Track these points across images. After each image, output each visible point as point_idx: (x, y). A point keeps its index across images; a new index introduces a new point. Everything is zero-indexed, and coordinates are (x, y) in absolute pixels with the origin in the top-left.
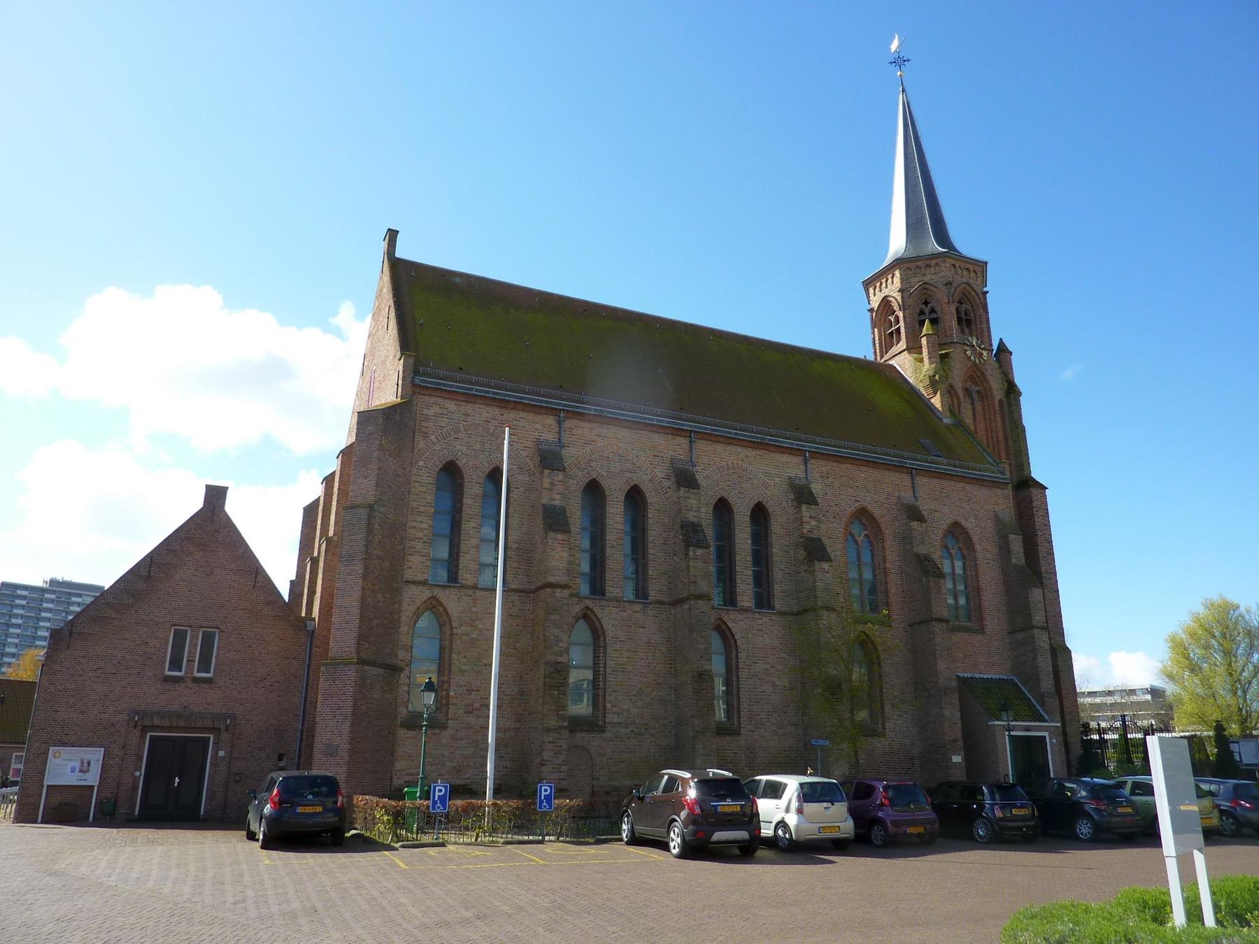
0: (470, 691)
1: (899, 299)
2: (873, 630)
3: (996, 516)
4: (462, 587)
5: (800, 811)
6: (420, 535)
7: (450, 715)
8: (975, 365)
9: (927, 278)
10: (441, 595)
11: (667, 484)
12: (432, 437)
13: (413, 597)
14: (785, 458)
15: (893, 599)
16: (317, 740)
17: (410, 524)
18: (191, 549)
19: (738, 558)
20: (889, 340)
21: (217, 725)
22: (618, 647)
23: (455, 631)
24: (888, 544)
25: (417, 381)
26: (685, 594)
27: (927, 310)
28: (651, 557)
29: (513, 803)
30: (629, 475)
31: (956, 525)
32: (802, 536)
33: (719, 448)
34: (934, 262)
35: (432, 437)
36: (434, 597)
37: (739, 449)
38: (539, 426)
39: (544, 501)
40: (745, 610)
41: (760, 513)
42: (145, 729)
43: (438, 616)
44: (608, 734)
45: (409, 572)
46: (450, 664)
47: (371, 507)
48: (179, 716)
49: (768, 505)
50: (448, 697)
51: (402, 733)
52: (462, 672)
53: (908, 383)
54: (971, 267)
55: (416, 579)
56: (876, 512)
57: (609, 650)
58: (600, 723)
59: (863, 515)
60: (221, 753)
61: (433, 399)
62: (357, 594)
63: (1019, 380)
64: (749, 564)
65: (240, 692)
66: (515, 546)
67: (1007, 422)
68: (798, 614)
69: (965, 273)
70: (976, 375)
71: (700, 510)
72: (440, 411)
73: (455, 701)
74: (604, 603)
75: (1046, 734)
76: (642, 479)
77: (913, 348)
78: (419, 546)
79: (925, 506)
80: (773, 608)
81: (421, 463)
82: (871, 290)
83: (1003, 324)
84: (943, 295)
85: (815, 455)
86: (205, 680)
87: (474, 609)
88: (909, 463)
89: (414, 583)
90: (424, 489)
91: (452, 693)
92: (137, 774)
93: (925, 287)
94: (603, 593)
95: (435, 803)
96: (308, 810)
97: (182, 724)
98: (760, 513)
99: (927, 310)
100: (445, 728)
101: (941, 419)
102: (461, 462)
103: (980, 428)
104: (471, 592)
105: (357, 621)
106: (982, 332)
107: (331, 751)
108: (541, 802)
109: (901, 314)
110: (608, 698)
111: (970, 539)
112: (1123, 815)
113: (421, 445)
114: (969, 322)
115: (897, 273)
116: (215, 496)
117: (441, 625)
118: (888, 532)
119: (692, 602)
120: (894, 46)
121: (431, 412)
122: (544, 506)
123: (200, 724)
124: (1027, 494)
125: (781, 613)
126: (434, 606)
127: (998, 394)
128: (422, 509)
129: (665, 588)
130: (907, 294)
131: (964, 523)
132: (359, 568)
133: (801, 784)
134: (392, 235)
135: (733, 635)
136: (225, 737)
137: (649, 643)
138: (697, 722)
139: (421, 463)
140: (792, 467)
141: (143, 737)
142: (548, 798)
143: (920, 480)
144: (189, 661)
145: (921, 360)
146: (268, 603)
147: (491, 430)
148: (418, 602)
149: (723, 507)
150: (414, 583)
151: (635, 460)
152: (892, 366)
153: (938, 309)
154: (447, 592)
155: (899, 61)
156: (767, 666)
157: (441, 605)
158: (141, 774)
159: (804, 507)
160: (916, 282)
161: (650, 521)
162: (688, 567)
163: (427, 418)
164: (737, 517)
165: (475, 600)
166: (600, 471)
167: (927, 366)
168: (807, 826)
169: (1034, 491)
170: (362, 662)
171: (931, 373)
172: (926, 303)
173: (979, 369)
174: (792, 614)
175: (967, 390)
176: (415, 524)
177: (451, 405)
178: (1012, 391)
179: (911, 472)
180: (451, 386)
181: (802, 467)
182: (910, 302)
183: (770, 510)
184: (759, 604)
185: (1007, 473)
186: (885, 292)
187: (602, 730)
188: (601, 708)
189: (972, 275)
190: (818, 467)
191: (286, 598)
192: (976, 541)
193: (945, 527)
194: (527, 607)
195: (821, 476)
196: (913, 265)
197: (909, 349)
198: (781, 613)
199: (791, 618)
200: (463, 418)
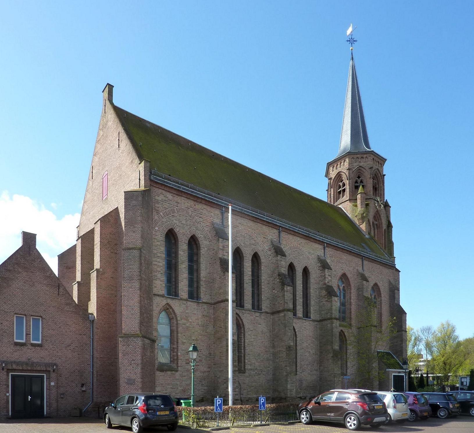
1: (347, 173)
2: (345, 330)
3: (390, 282)
4: (181, 299)
5: (395, 407)
6: (159, 269)
7: (179, 365)
9: (361, 164)
11: (269, 253)
12: (161, 214)
13: (159, 303)
14: (317, 246)
15: (353, 316)
17: (154, 263)
18: (20, 270)
20: (340, 193)
21: (48, 369)
22: (250, 333)
23: (179, 322)
25: (152, 178)
26: (281, 309)
27: (359, 181)
29: (273, 405)
30: (254, 246)
31: (376, 285)
32: (325, 284)
33: (291, 237)
34: (365, 156)
35: (161, 214)
36: (167, 304)
37: (299, 239)
38: (212, 214)
39: (220, 256)
40: (299, 318)
41: (306, 271)
42: (8, 371)
44: (247, 374)
45: (155, 289)
46: (177, 339)
47: (140, 249)
48: (27, 364)
49: (259, 254)
50: (177, 355)
51: (158, 373)
52: (183, 343)
53: (348, 217)
55: (159, 293)
56: (349, 276)
57: (246, 335)
58: (243, 369)
60: (52, 384)
61: (160, 191)
62: (137, 299)
63: (392, 221)
65: (57, 352)
66: (204, 279)
67: (387, 240)
68: (321, 321)
69: (377, 164)
70: (377, 216)
72: (164, 198)
73: (181, 358)
74: (244, 311)
77: (353, 199)
80: (310, 318)
81: (157, 228)
82: (331, 168)
83: (391, 193)
84: (364, 172)
85: (329, 245)
86: (38, 345)
87: (187, 311)
88: (362, 253)
89: (158, 295)
90: (159, 243)
91: (179, 354)
92: (8, 394)
93: (360, 169)
95: (217, 407)
96: (162, 413)
97: (29, 368)
98: (306, 271)
99: (359, 181)
100: (177, 371)
101: (365, 235)
102: (177, 230)
103: (376, 241)
104: (185, 302)
105: (139, 314)
106: (381, 195)
107: (131, 382)
108: (261, 406)
109: (347, 182)
110: (246, 358)
111: (380, 291)
113: (156, 218)
115: (347, 160)
116: (29, 239)
117: (170, 319)
118: (352, 285)
119: (286, 313)
120: (349, 31)
121: (159, 198)
122: (220, 259)
123: (39, 368)
125: (314, 321)
126: (168, 309)
127: (384, 227)
128: (159, 255)
129: (269, 306)
130: (351, 171)
132: (137, 285)
133: (394, 395)
134: (110, 87)
136: (53, 375)
137: (262, 332)
138: (288, 369)
139: (157, 228)
140: (317, 250)
141: (8, 375)
142: (263, 404)
144: (27, 334)
145: (356, 206)
146: (67, 304)
147: (190, 214)
148: (161, 306)
150: (158, 295)
151: (256, 239)
152: (340, 208)
153: (364, 181)
154: (174, 301)
155: (352, 41)
157: (171, 308)
158: (9, 394)
159: (326, 270)
160: (356, 165)
161: (263, 272)
162: (284, 295)
163: (158, 202)
164: (297, 273)
165: (187, 307)
167: (360, 209)
168: (399, 413)
170: (144, 337)
171: (362, 212)
172: (359, 177)
173: (378, 213)
174: (317, 321)
175: (373, 222)
176: (156, 263)
177: (169, 196)
178: (389, 226)
179: (363, 258)
180: (170, 184)
181: (323, 251)
182: (352, 176)
183: (310, 271)
186: (339, 169)
189: (380, 165)
190: (329, 251)
191: (77, 302)
192: (382, 293)
194: (211, 311)
195: (331, 256)
196: (355, 156)
197: (350, 200)
198: (314, 321)
199: (316, 323)
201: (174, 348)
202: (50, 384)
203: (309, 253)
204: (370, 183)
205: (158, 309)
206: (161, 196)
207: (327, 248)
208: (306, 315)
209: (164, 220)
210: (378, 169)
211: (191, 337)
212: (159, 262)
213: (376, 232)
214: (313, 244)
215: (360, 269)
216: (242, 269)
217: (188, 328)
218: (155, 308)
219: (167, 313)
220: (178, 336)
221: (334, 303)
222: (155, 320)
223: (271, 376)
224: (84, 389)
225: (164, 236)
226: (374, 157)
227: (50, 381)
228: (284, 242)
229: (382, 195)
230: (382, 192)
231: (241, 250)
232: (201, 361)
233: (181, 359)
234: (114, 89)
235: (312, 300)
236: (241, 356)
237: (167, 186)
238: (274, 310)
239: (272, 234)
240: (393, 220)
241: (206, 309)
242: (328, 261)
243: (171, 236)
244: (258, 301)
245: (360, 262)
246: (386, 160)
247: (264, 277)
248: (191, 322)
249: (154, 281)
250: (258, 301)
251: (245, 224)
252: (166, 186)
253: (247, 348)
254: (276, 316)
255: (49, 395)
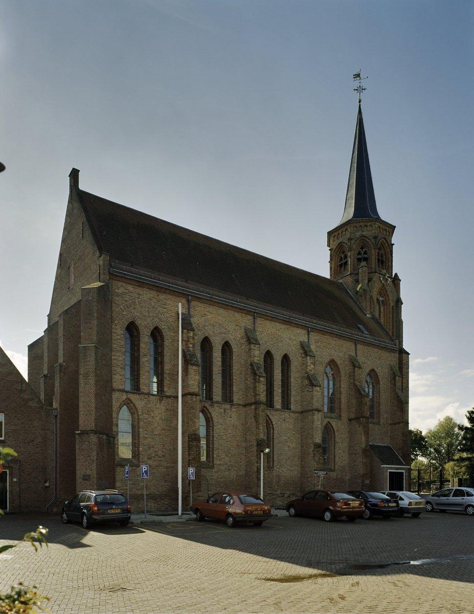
0: (149, 448)
7: (141, 460)
8: (383, 285)
9: (364, 233)
10: (131, 396)
14: (299, 331)
15: (343, 406)
16: (78, 472)
19: (275, 383)
24: (342, 378)
28: (234, 381)
31: (373, 370)
32: (307, 373)
33: (268, 323)
37: (277, 324)
41: (286, 359)
43: (130, 409)
49: (290, 356)
54: (387, 228)
56: (338, 362)
59: (332, 363)
60: (15, 480)
61: (120, 283)
64: (280, 387)
66: (168, 372)
68: (302, 412)
69: (384, 232)
71: (258, 355)
75: (404, 471)
76: (231, 338)
78: (119, 370)
79: (361, 359)
80: (290, 409)
84: (364, 241)
87: (149, 406)
90: (119, 337)
91: (141, 449)
94: (273, 407)
98: (286, 359)
102: (138, 322)
104: (146, 397)
112: (392, 507)
114: (382, 261)
117: (132, 414)
118: (342, 372)
124: (403, 355)
131: (376, 369)
135: (272, 422)
140: (300, 335)
143: (359, 346)
149: (268, 355)
156: (286, 438)
157: (132, 402)
163: (118, 295)
166: (209, 332)
169: (404, 355)
172: (362, 248)
176: (115, 357)
177: (130, 288)
178: (399, 302)
179: (356, 342)
181: (307, 336)
183: (291, 358)
184: (283, 407)
185: (397, 345)
187: (212, 467)
188: (211, 456)
189: (388, 233)
190: (314, 336)
193: (368, 371)
195: (316, 342)
200: (137, 296)
201: (135, 443)
202: (12, 480)
203: (290, 339)
204: (373, 254)
205: (118, 404)
206: (120, 288)
207: (311, 333)
208: (286, 405)
209: (125, 313)
210: (385, 239)
211: (153, 432)
212: (119, 356)
213: (382, 309)
214: (295, 329)
215: (353, 354)
216: (211, 360)
217: (149, 423)
218: (114, 403)
219: (128, 407)
220: (139, 431)
221: (315, 393)
222: (114, 415)
223: (243, 472)
224: (47, 484)
225: (124, 329)
226: (379, 225)
227: (12, 477)
228: (259, 329)
229: (390, 268)
230: (333, 267)
231: (229, 343)
232: (164, 456)
233: (143, 455)
234: (80, 173)
235: (292, 390)
236: (210, 451)
237: (127, 278)
238: (247, 402)
239: (246, 321)
240: (403, 296)
241: (170, 402)
242: (313, 347)
243: (132, 329)
244: (230, 392)
245: (353, 346)
246: (395, 227)
247: (236, 368)
248: (153, 417)
249: (113, 376)
250: (230, 392)
251: (214, 312)
252: (126, 278)
253: (215, 442)
254: (248, 408)
255: (11, 492)
